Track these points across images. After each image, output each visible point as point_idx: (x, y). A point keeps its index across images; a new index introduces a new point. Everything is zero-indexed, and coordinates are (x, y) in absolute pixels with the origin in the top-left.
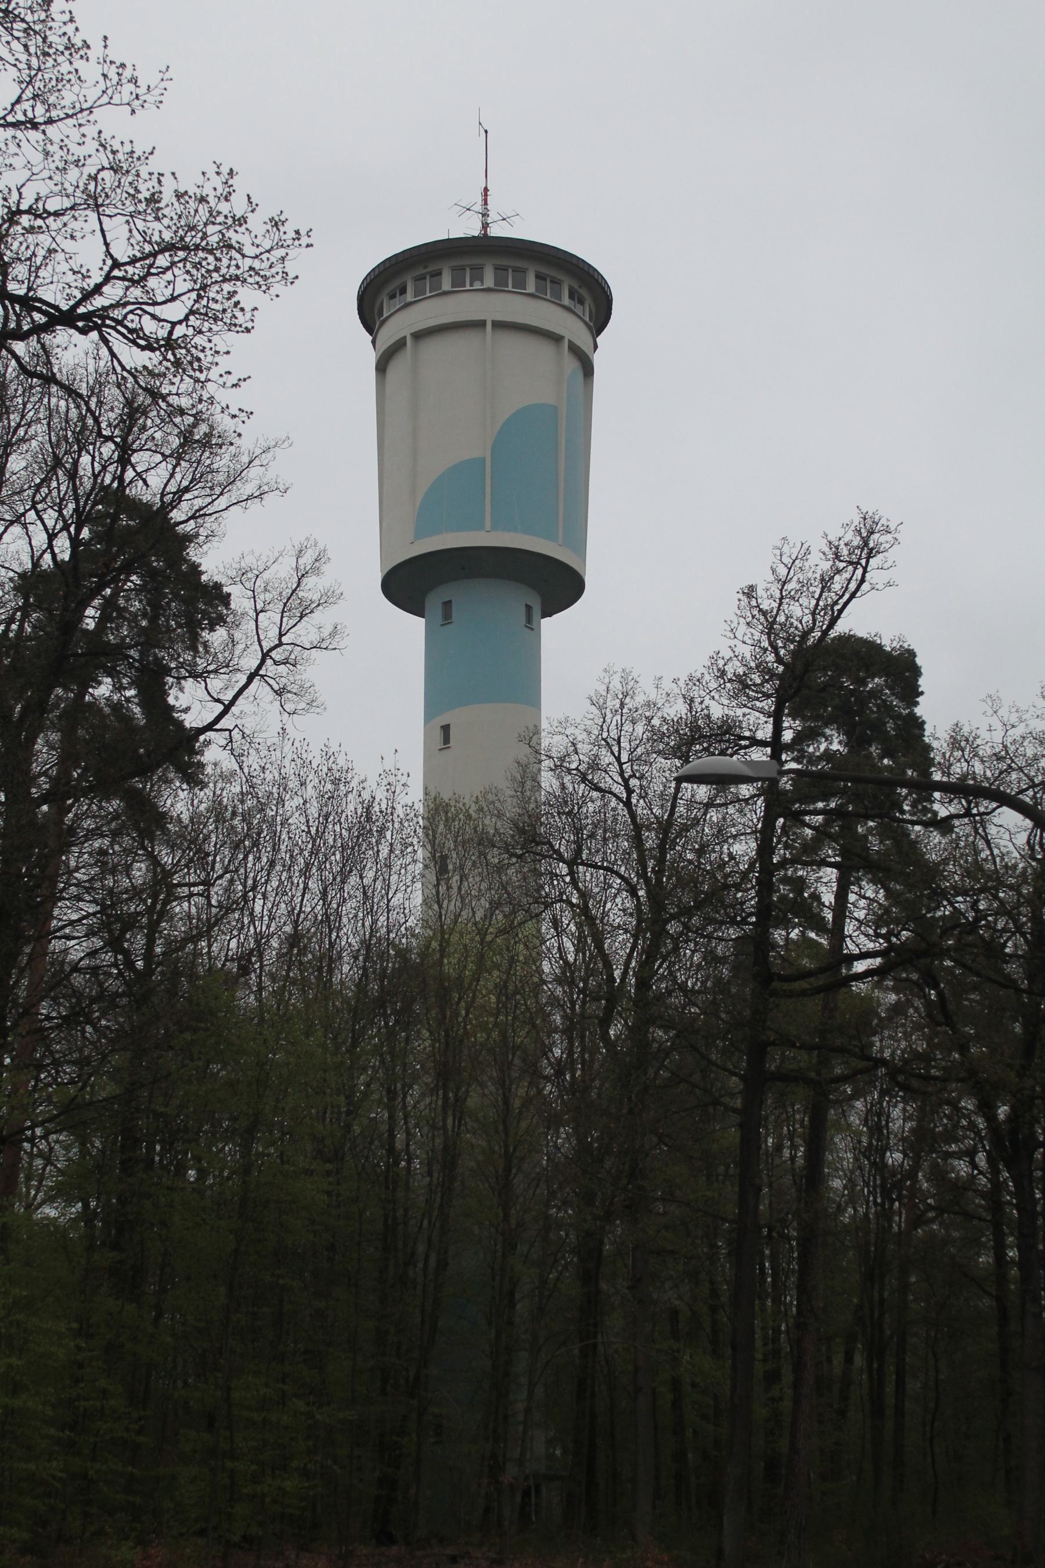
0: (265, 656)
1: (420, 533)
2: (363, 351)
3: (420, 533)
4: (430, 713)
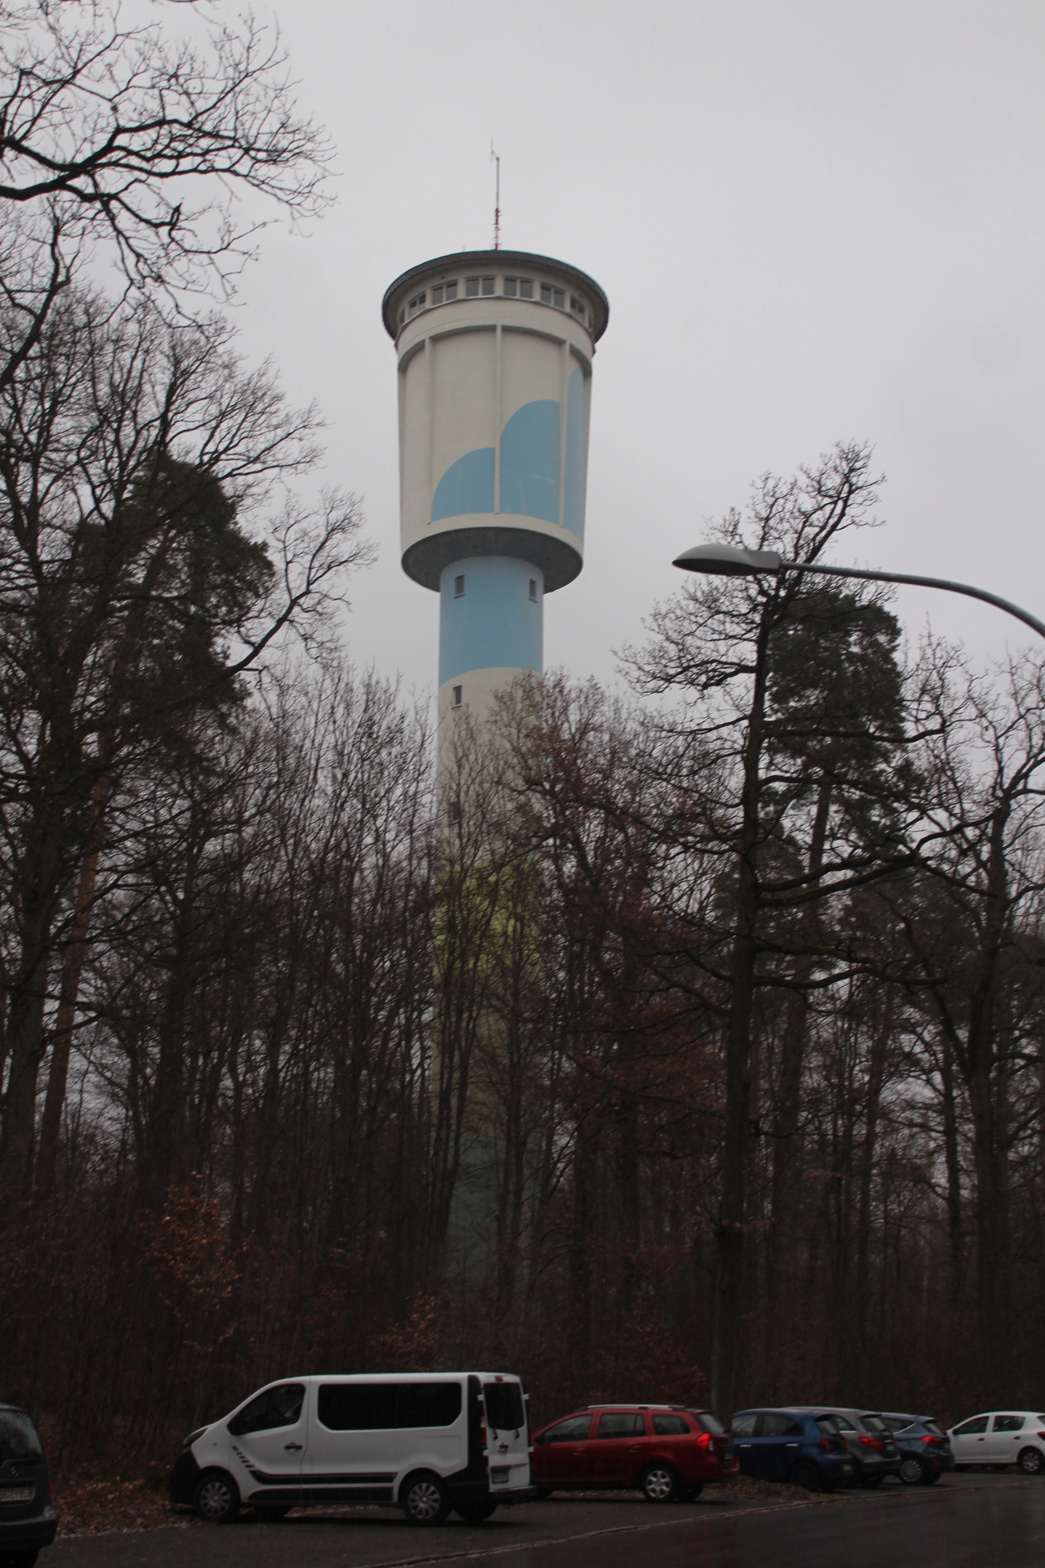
0: (294, 602)
1: (436, 515)
2: (385, 353)
3: (436, 515)
4: (445, 675)
